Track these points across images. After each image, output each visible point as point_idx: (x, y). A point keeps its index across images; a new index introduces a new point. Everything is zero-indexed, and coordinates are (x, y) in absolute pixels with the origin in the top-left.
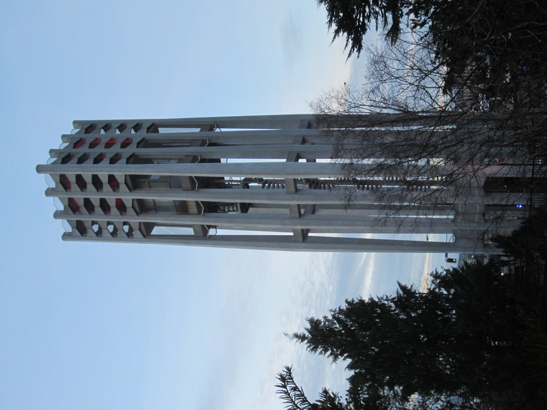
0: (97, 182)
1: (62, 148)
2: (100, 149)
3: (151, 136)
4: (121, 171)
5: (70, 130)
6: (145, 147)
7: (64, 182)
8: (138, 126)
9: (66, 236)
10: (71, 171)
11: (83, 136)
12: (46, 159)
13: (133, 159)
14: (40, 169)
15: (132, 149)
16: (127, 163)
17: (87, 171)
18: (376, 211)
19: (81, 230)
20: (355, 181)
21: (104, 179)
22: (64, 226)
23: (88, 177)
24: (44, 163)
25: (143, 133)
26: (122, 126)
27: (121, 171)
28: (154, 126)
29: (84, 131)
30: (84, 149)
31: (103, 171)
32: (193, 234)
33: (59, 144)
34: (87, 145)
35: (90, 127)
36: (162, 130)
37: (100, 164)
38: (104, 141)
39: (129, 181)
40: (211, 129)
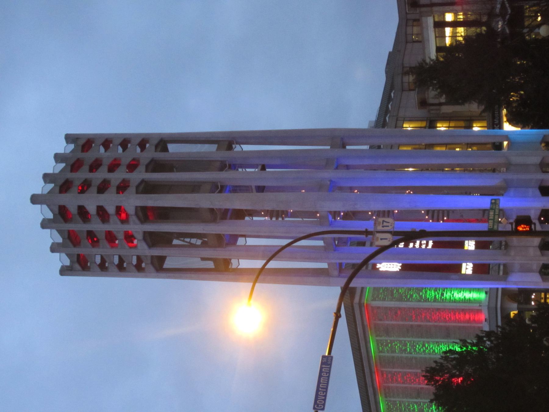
0: (102, 213)
1: (57, 171)
2: (102, 174)
3: (161, 156)
4: (132, 201)
5: (62, 147)
6: (154, 170)
7: (63, 213)
8: (143, 142)
9: (65, 271)
10: (72, 201)
11: (80, 155)
12: (40, 187)
13: (147, 188)
14: (35, 199)
15: (139, 175)
16: (118, 192)
17: (91, 201)
18: (428, 230)
19: (80, 265)
20: (446, 145)
21: (111, 210)
22: (59, 260)
23: (92, 209)
24: (39, 192)
25: (150, 153)
26: (125, 142)
27: (132, 201)
28: (162, 143)
29: (80, 148)
30: (83, 174)
31: (110, 201)
32: (213, 267)
33: (51, 166)
34: (86, 168)
35: (84, 143)
36: (172, 148)
37: (126, 193)
38: (106, 162)
39: (140, 214)
40: (230, 147)
